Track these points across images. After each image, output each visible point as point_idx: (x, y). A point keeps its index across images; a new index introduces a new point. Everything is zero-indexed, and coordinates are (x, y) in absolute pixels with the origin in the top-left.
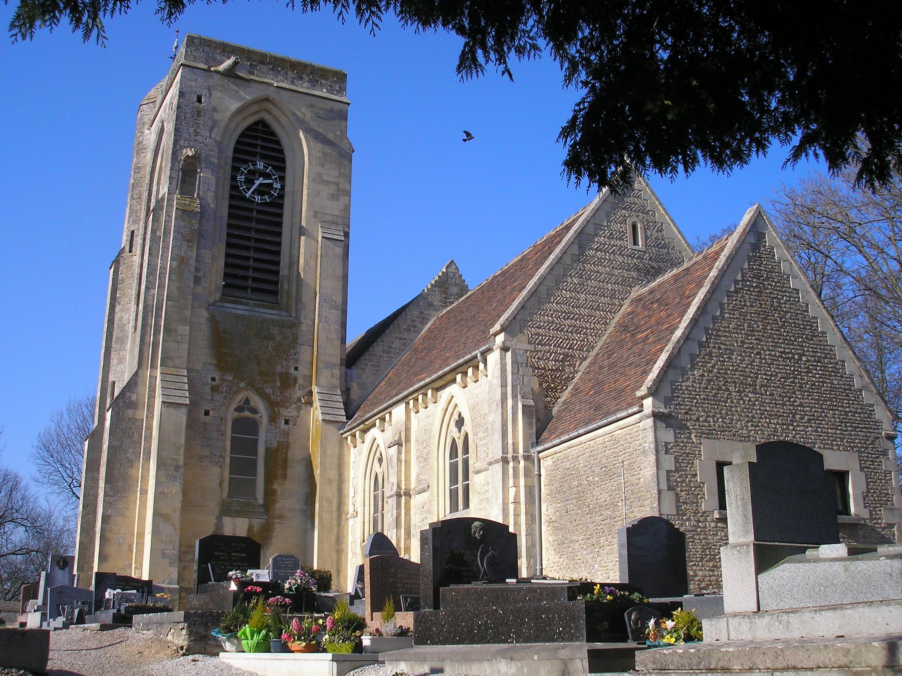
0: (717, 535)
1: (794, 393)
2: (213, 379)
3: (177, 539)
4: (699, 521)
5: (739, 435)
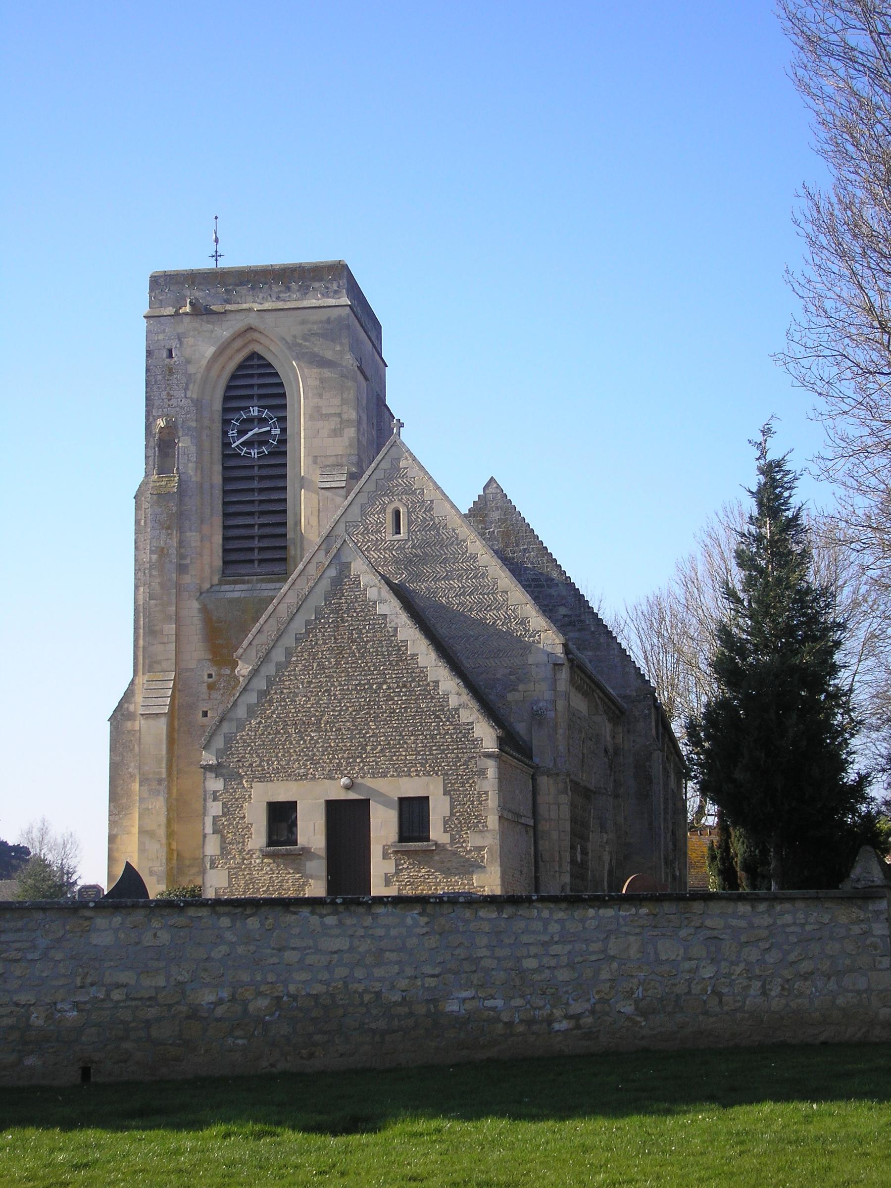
0: (262, 870)
1: (368, 724)
2: (210, 676)
3: (163, 855)
4: (244, 859)
5: (295, 775)
